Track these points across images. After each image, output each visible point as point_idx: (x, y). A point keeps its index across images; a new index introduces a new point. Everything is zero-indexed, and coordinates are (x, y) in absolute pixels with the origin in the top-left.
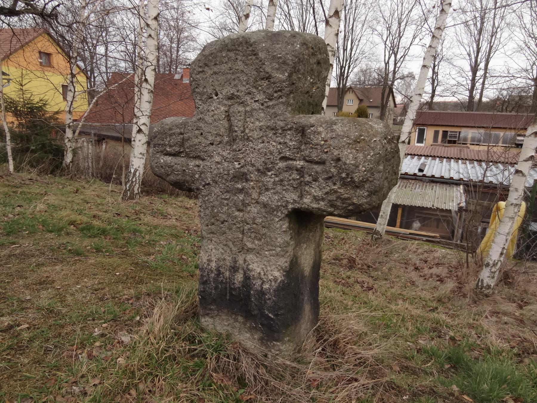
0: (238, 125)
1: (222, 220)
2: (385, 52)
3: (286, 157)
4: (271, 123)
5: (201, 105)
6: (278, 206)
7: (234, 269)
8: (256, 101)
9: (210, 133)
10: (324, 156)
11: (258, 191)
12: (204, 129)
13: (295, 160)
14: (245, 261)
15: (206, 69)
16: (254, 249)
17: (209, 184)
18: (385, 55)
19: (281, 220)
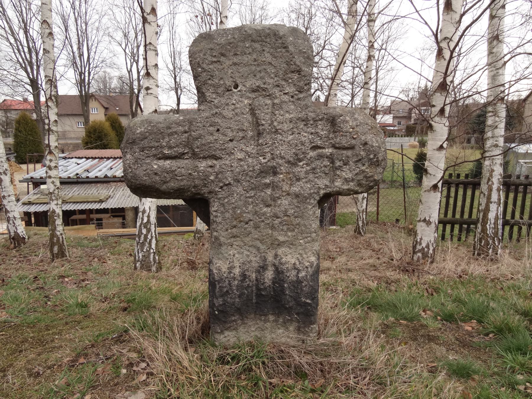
0: (265, 117)
1: (247, 220)
2: (126, 60)
3: (317, 146)
4: (302, 115)
5: (215, 99)
6: (311, 193)
8: (285, 94)
9: (230, 128)
10: (353, 142)
11: (289, 182)
12: (222, 124)
13: (324, 148)
14: (276, 256)
15: (222, 59)
16: (287, 241)
17: (230, 184)
18: (127, 63)
19: (314, 207)
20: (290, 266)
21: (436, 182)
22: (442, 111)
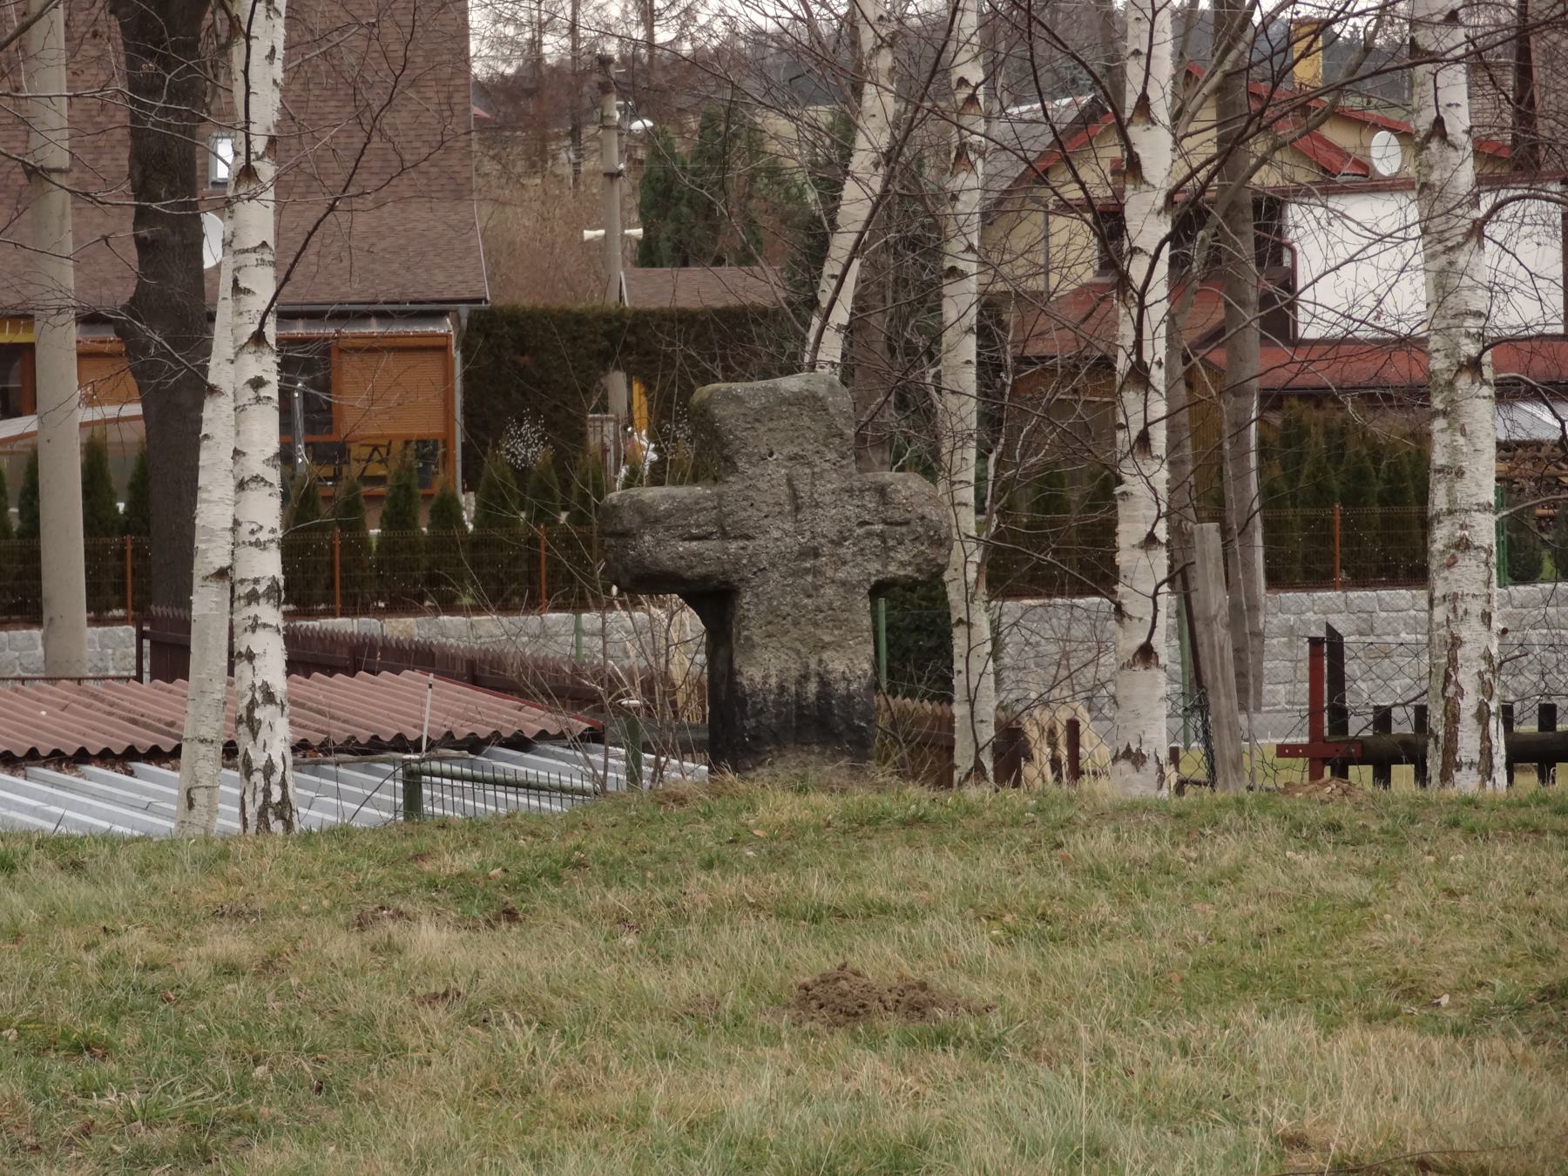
0: (803, 489)
7: (804, 678)
14: (820, 661)
20: (838, 676)
21: (1144, 640)
22: (1144, 440)
